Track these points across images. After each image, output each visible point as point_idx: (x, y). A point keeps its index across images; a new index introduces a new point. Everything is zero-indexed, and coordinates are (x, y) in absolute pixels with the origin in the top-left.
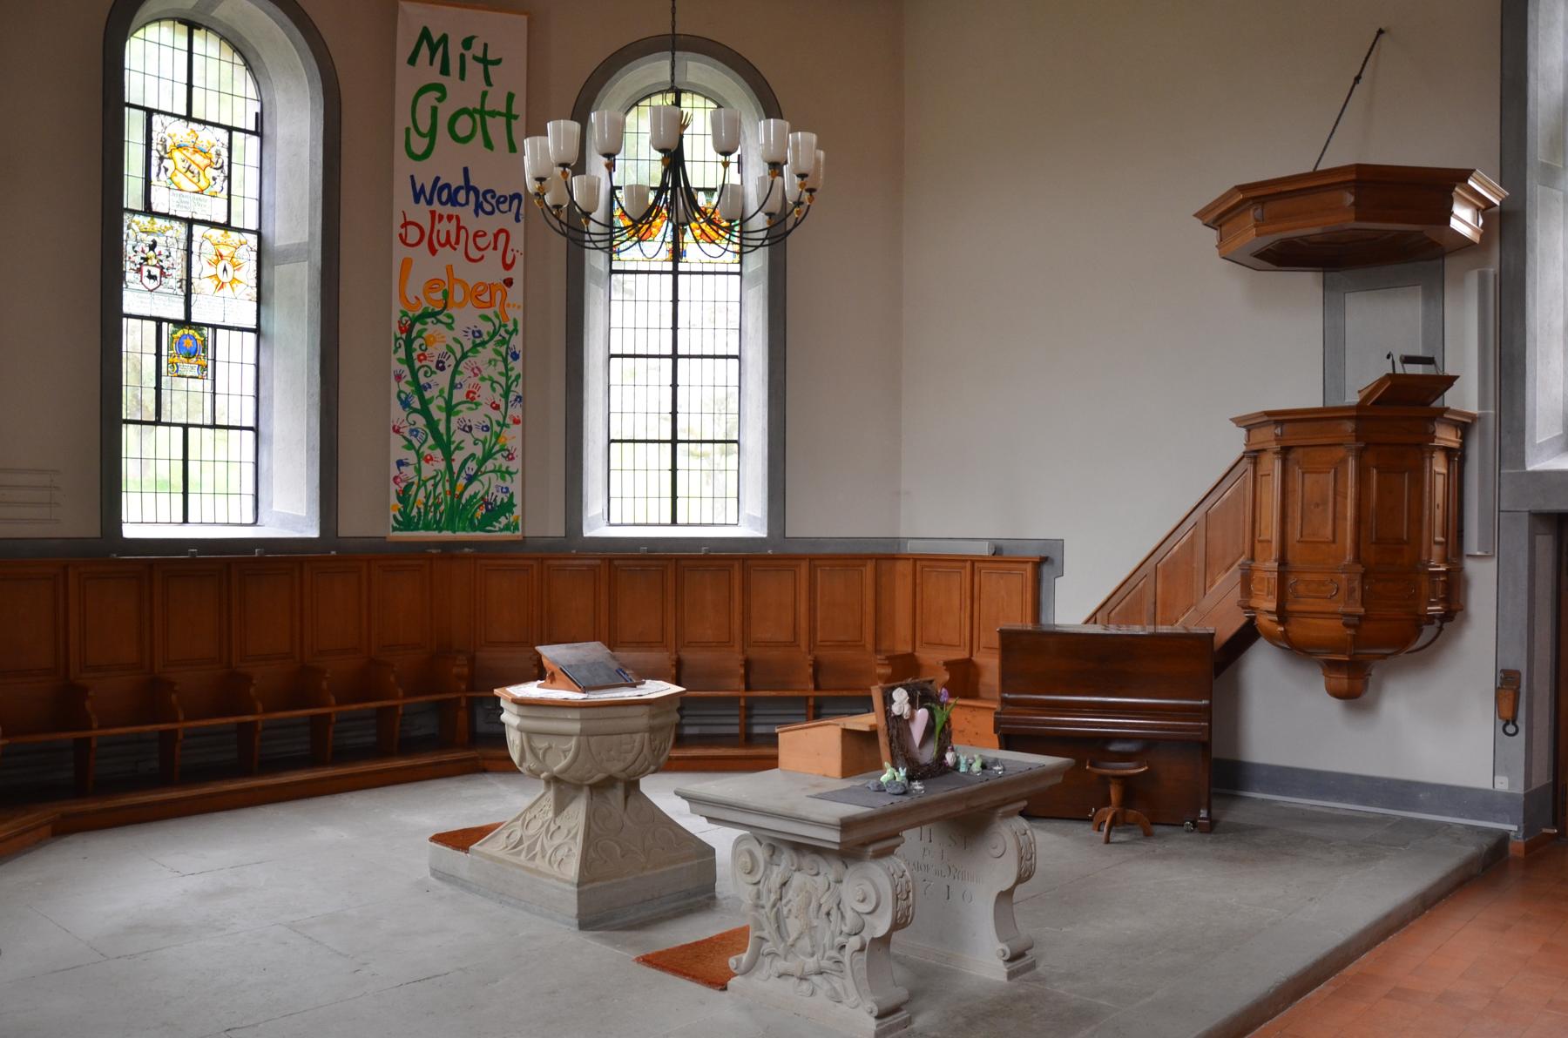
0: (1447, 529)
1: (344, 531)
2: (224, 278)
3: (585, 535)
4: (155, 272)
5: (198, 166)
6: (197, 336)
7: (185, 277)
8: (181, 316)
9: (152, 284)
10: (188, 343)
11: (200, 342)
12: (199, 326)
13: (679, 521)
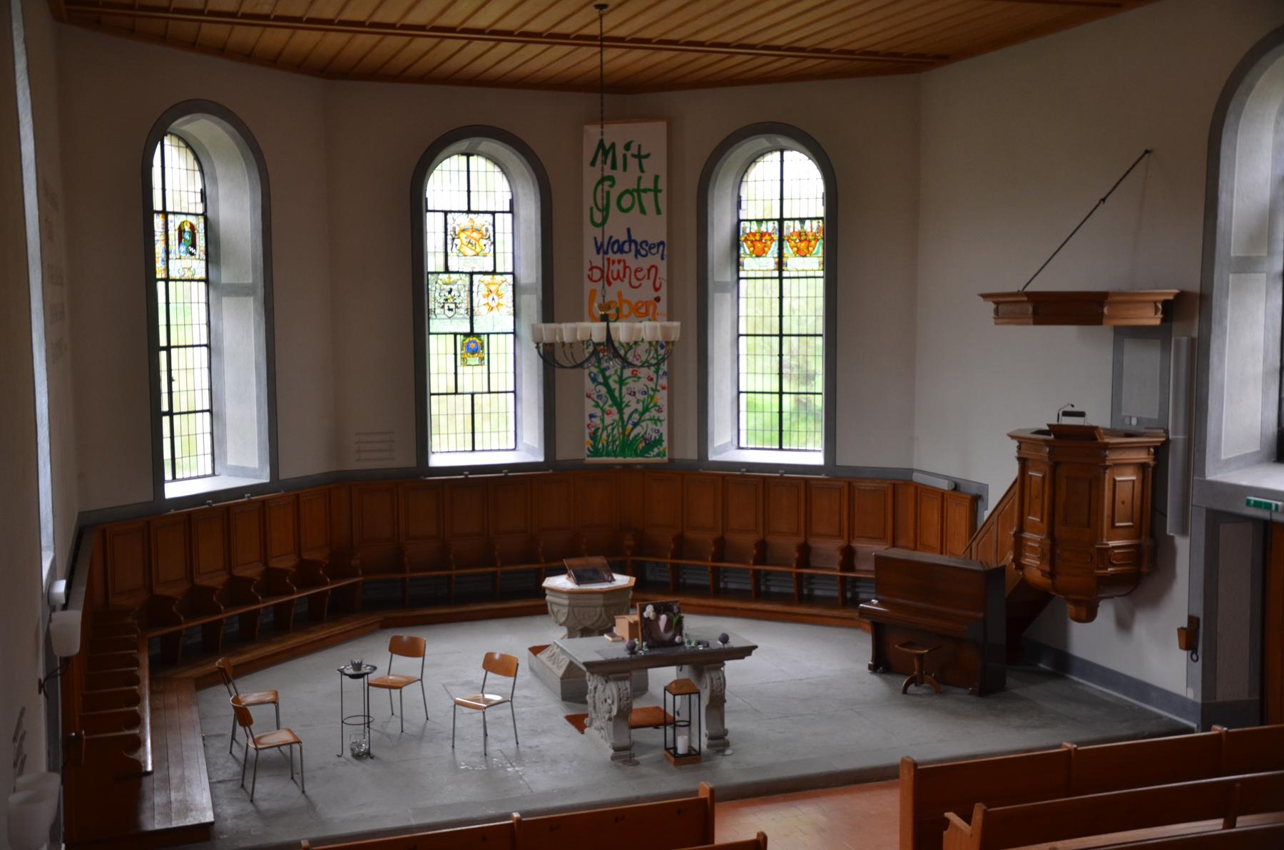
2: (493, 304)
4: (452, 306)
5: (475, 239)
6: (478, 341)
7: (469, 307)
8: (468, 330)
9: (450, 314)
10: (473, 346)
11: (479, 345)
12: (478, 335)
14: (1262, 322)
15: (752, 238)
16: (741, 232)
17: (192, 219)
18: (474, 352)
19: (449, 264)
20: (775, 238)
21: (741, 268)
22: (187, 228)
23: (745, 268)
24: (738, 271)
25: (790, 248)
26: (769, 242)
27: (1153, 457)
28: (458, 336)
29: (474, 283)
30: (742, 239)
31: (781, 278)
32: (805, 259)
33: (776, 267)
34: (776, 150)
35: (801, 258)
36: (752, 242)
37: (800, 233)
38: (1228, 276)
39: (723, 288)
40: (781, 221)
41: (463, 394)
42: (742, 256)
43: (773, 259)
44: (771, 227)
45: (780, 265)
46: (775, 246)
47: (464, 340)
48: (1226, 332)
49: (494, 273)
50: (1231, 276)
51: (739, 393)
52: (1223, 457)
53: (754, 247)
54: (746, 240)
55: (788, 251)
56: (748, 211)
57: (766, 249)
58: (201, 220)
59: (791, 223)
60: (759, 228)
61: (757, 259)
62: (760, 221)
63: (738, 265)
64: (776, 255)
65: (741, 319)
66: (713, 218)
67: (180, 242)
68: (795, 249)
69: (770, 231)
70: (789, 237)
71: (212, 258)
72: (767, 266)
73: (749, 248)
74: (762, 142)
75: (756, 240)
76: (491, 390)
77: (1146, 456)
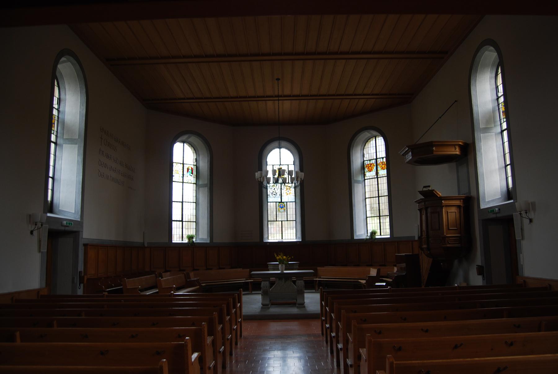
1: (214, 241)
2: (288, 193)
3: (355, 238)
4: (275, 194)
8: (280, 201)
9: (274, 196)
10: (282, 206)
12: (283, 202)
13: (382, 235)
14: (496, 150)
15: (368, 166)
17: (193, 167)
21: (365, 176)
22: (190, 168)
24: (364, 177)
26: (373, 167)
27: (462, 203)
28: (277, 203)
30: (365, 166)
31: (377, 178)
34: (374, 137)
36: (368, 167)
39: (358, 182)
40: (376, 159)
41: (279, 221)
44: (374, 161)
45: (377, 173)
46: (375, 168)
48: (482, 154)
50: (481, 134)
51: (367, 218)
52: (487, 201)
54: (366, 167)
55: (379, 169)
56: (367, 157)
57: (372, 169)
58: (195, 167)
59: (379, 159)
60: (370, 162)
62: (370, 160)
63: (364, 175)
64: (375, 170)
65: (366, 193)
66: (353, 160)
67: (188, 172)
68: (381, 168)
69: (373, 163)
71: (197, 177)
73: (367, 169)
74: (366, 134)
75: (369, 166)
77: (460, 203)
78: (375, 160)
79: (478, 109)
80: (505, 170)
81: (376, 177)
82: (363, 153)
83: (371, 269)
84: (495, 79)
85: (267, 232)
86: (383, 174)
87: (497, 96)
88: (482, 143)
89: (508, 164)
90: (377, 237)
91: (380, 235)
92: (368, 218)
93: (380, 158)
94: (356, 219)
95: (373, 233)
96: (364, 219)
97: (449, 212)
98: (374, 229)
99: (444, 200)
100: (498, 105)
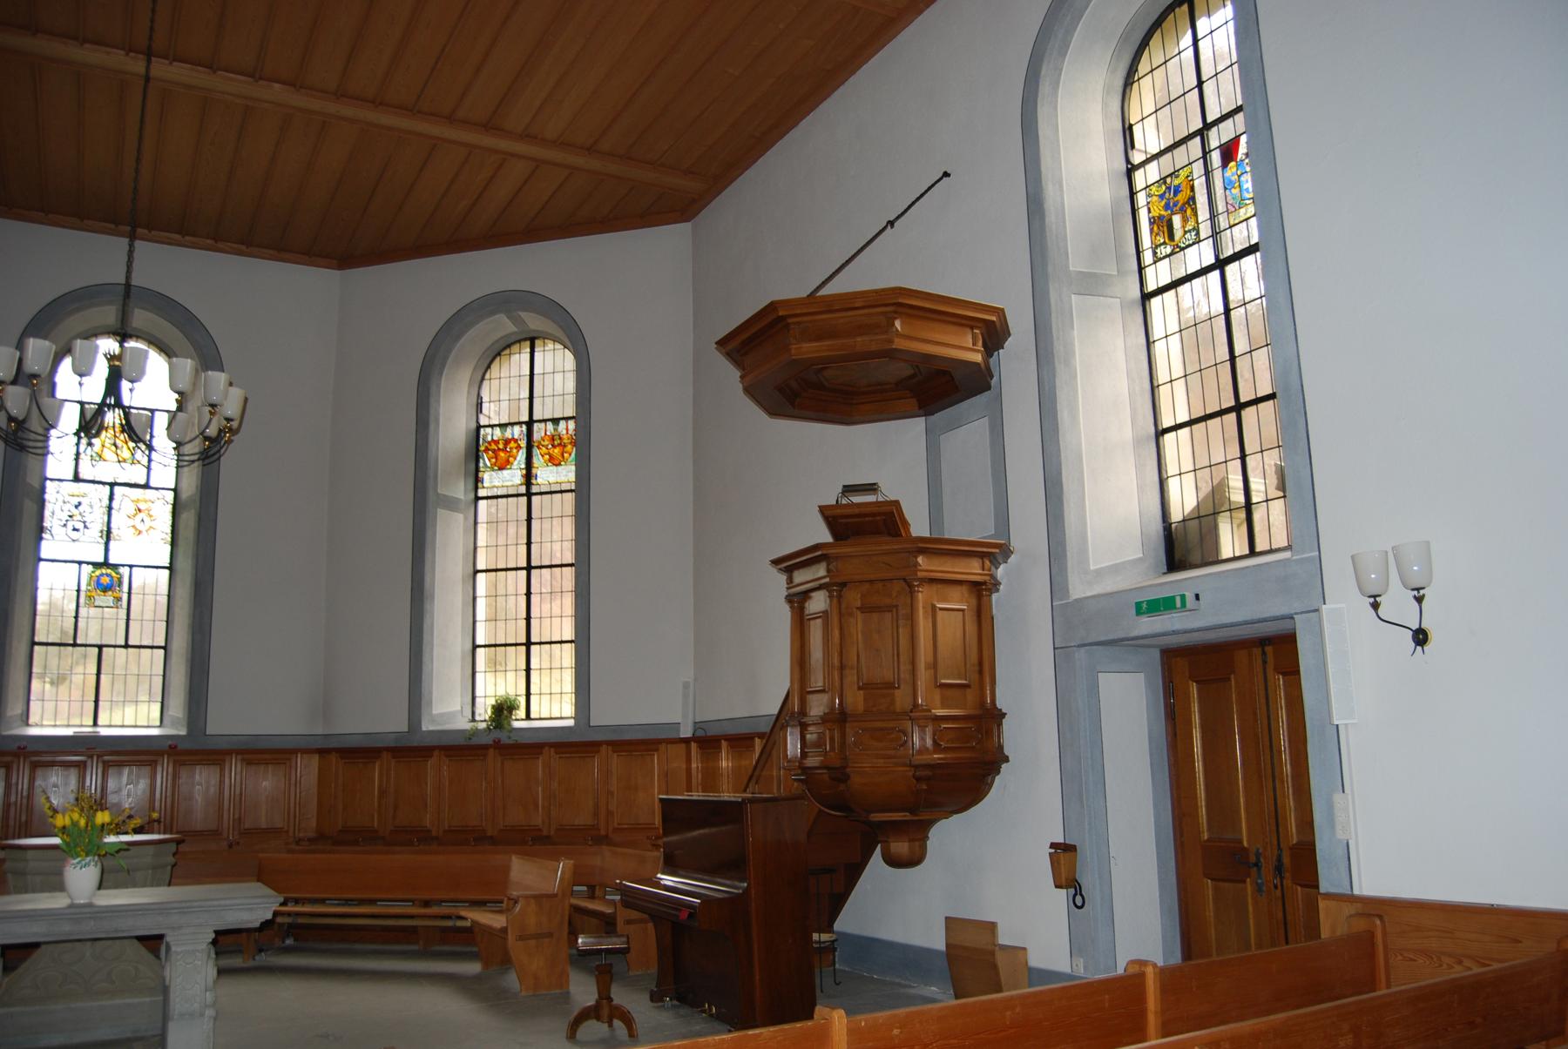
0: (138, 761)
2: (140, 526)
3: (424, 729)
4: (80, 526)
6: (114, 574)
7: (105, 529)
9: (75, 535)
10: (105, 580)
11: (115, 579)
12: (115, 567)
13: (532, 716)
14: (1123, 366)
15: (494, 447)
16: (481, 440)
18: (106, 589)
19: (80, 470)
20: (522, 446)
21: (480, 485)
23: (485, 485)
24: (476, 488)
25: (540, 456)
26: (515, 451)
29: (115, 497)
30: (482, 448)
31: (529, 495)
32: (560, 468)
33: (523, 480)
34: (525, 339)
35: (555, 467)
37: (553, 436)
38: (1071, 297)
39: (451, 504)
40: (530, 424)
42: (482, 469)
43: (519, 471)
44: (518, 432)
45: (529, 477)
46: (521, 456)
47: (93, 572)
49: (146, 486)
51: (475, 647)
52: (1092, 568)
53: (496, 458)
54: (487, 450)
55: (538, 461)
56: (493, 413)
57: (511, 459)
61: (499, 472)
62: (503, 426)
63: (477, 481)
64: (523, 466)
68: (547, 457)
69: (516, 437)
70: (539, 442)
72: (512, 481)
75: (499, 449)
76: (130, 643)
78: (524, 427)
79: (1063, 198)
80: (1155, 449)
81: (523, 490)
82: (479, 398)
83: (514, 858)
84: (1120, 98)
85: (21, 693)
86: (552, 480)
87: (1128, 161)
88: (1075, 332)
89: (1165, 427)
90: (516, 724)
91: (524, 717)
92: (478, 650)
93: (545, 421)
94: (432, 649)
95: (503, 710)
96: (463, 652)
97: (941, 609)
98: (501, 692)
99: (923, 551)
100: (1132, 194)
